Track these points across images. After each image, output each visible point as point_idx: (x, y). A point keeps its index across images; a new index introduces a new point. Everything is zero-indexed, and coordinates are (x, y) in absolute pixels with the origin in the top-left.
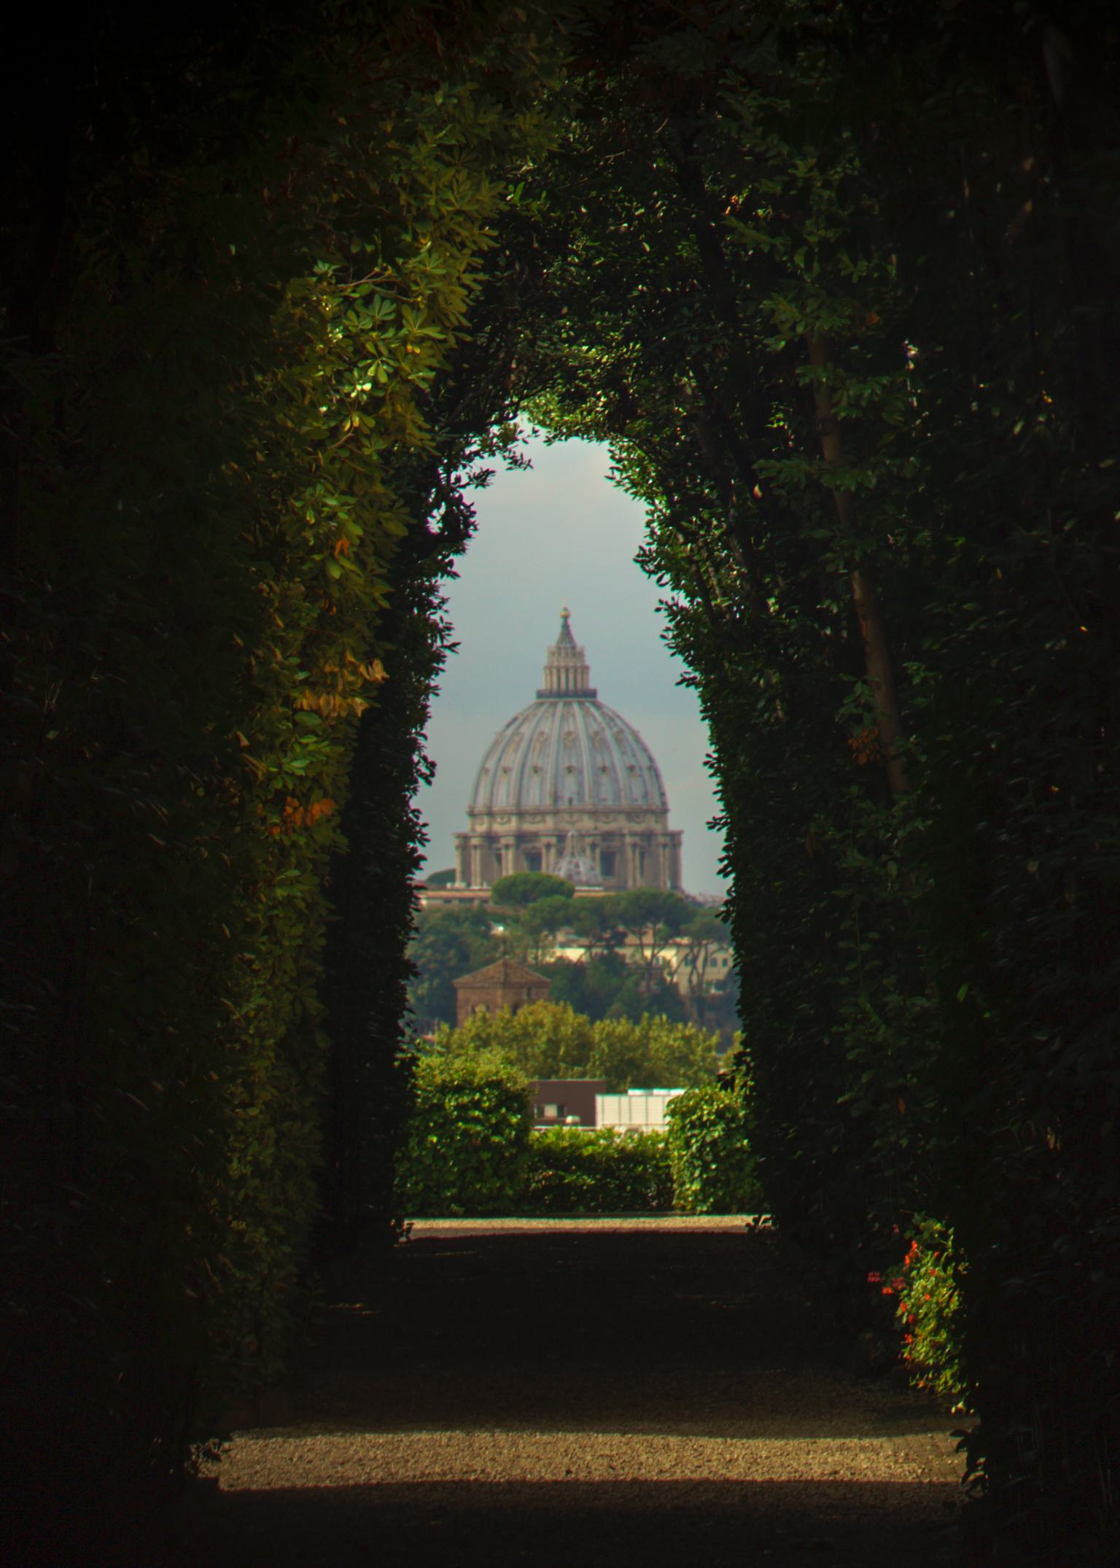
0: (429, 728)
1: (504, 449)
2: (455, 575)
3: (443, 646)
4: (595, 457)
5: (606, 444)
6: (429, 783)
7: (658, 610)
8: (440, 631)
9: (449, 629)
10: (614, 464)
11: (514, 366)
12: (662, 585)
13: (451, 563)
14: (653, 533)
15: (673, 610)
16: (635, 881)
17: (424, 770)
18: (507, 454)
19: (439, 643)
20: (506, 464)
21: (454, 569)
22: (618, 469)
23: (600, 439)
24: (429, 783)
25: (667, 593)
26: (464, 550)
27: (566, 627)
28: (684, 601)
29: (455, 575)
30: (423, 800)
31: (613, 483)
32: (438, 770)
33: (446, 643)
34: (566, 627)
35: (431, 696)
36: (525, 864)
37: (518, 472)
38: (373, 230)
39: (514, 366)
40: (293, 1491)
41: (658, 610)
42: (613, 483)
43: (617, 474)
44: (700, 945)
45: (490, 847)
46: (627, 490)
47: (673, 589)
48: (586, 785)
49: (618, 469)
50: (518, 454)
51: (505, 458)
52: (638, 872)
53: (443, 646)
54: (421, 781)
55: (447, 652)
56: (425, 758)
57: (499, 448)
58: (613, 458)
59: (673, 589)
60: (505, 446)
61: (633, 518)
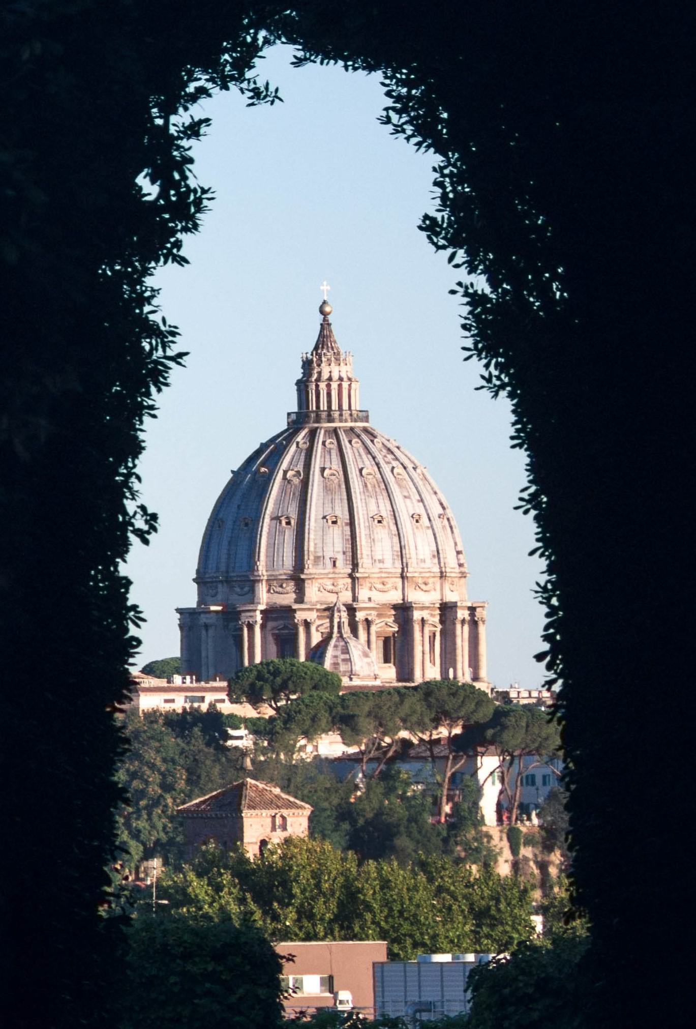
0: (143, 464)
1: (240, 78)
3: (166, 357)
4: (363, 92)
6: (146, 542)
7: (453, 292)
8: (164, 335)
9: (174, 334)
10: (389, 102)
13: (178, 245)
14: (444, 197)
15: (475, 300)
16: (427, 670)
17: (140, 523)
18: (244, 85)
19: (160, 352)
20: (245, 98)
21: (182, 253)
22: (393, 109)
23: (370, 68)
24: (146, 542)
25: (462, 274)
26: (196, 227)
27: (325, 326)
31: (390, 128)
32: (161, 524)
33: (169, 353)
34: (325, 326)
35: (146, 418)
36: (273, 649)
37: (263, 107)
40: (243, 832)
41: (453, 292)
42: (390, 128)
43: (395, 117)
45: (226, 627)
46: (408, 139)
47: (470, 273)
48: (202, 799)
49: (393, 109)
50: (261, 84)
51: (242, 90)
52: (427, 656)
53: (166, 357)
56: (143, 508)
57: (232, 78)
59: (470, 273)
60: (242, 74)
61: (414, 176)
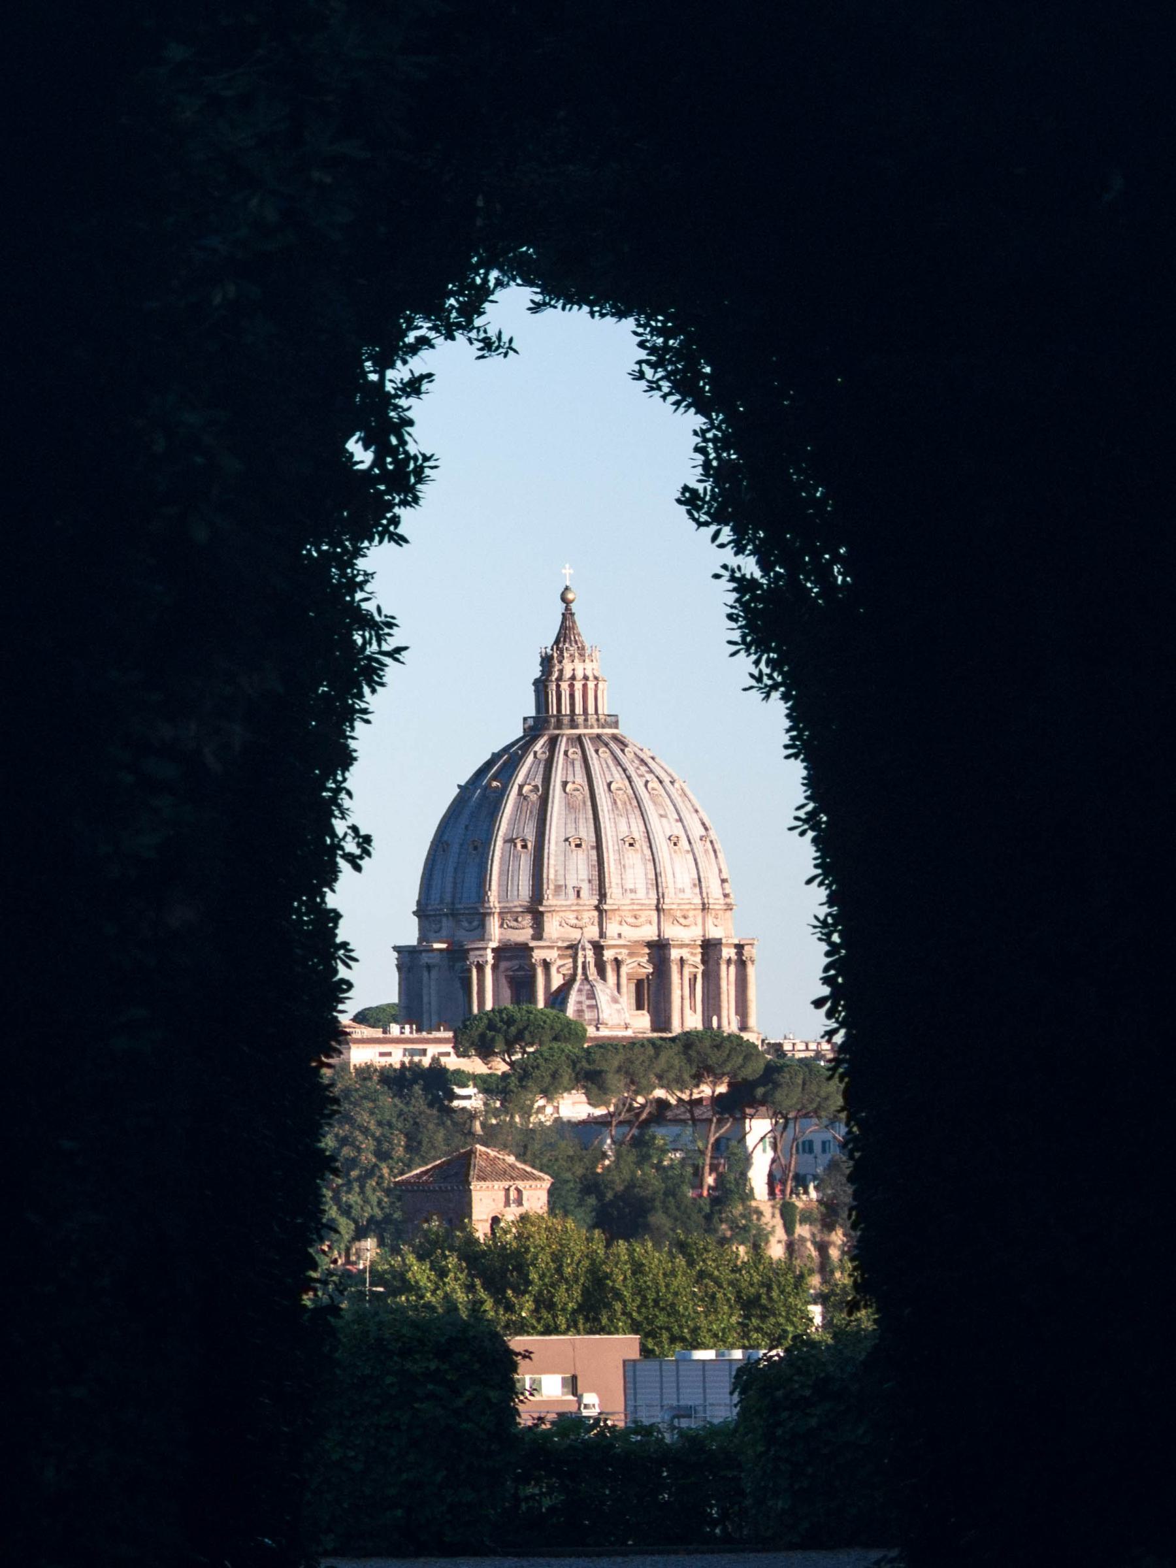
0: (354, 778)
1: (468, 326)
2: (400, 540)
5: (630, 323)
6: (358, 868)
7: (717, 576)
9: (390, 625)
11: (480, 203)
12: (722, 546)
13: (395, 521)
14: (707, 465)
16: (687, 1018)
17: (351, 847)
18: (473, 335)
20: (474, 350)
21: (400, 531)
22: (648, 362)
25: (727, 555)
26: (416, 500)
28: (750, 566)
29: (400, 540)
30: (347, 894)
31: (643, 384)
32: (375, 847)
33: (385, 647)
35: (358, 724)
38: (747, 1253)
39: (480, 203)
41: (717, 576)
42: (643, 384)
43: (649, 372)
44: (333, 1158)
49: (648, 362)
51: (470, 340)
54: (343, 864)
55: (387, 660)
56: (354, 829)
58: (641, 345)
59: (736, 554)
60: (470, 321)
61: (671, 441)
